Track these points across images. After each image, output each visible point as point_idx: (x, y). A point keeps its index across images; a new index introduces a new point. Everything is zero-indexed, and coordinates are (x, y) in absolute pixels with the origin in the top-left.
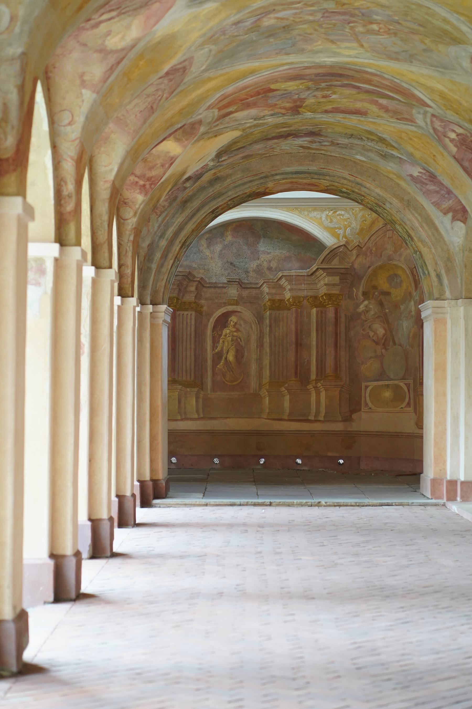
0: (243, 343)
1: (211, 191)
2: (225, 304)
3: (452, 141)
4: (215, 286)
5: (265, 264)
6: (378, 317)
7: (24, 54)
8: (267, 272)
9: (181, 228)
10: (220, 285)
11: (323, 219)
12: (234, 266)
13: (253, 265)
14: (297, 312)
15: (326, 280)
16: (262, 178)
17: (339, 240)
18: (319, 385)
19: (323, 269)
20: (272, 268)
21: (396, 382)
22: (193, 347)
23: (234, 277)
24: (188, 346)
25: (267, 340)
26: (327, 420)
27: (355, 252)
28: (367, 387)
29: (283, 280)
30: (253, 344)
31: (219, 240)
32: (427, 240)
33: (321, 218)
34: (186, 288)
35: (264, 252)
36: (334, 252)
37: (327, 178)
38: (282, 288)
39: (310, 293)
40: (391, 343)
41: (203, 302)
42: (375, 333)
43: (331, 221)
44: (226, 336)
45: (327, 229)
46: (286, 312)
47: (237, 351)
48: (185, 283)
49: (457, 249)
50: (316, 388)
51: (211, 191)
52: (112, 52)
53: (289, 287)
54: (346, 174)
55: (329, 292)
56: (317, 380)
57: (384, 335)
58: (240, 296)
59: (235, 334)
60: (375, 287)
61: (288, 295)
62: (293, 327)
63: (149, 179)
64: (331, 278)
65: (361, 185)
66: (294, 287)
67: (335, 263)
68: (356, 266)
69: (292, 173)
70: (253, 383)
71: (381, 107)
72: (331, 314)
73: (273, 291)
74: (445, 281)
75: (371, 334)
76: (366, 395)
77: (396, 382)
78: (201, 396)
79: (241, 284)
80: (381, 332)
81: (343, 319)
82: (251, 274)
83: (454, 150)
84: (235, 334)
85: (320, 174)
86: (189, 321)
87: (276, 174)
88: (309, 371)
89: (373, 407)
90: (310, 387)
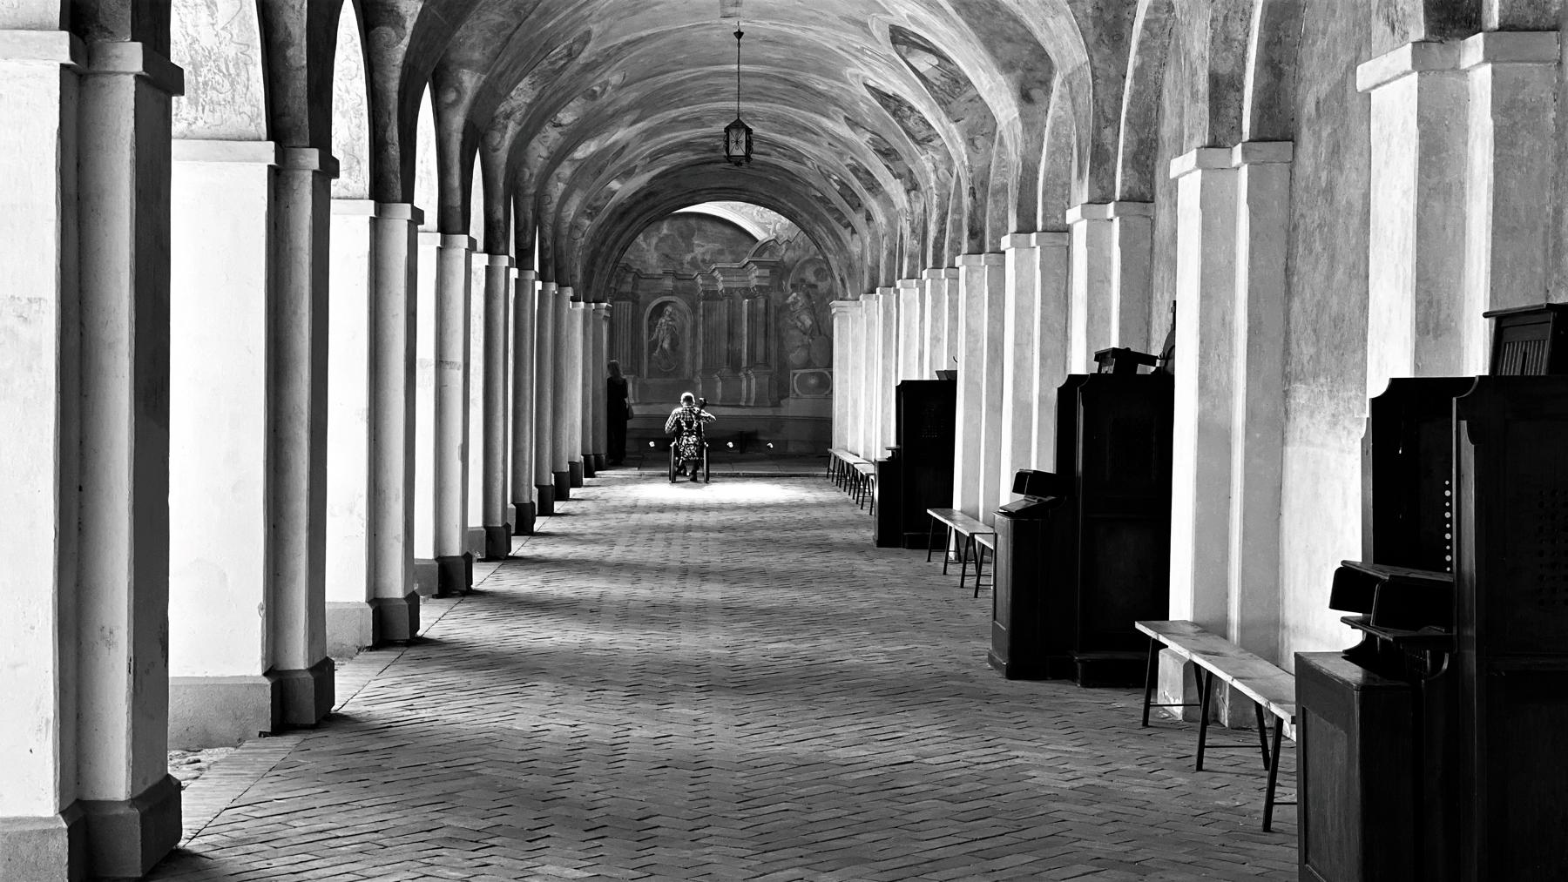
0: (677, 332)
1: (645, 205)
2: (661, 295)
3: (835, 181)
4: (511, 832)
5: (699, 257)
6: (806, 308)
7: (536, 192)
8: (701, 264)
9: (620, 236)
10: (656, 277)
11: (755, 214)
12: (670, 258)
13: (688, 257)
14: (729, 302)
15: (757, 273)
16: (690, 192)
17: (769, 234)
18: (750, 372)
19: (754, 262)
20: (705, 260)
21: (821, 370)
22: (630, 335)
23: (670, 269)
24: (625, 335)
25: (700, 329)
26: (759, 403)
27: (784, 246)
28: (794, 375)
29: (717, 272)
30: (688, 333)
31: (655, 233)
32: (832, 248)
33: (752, 214)
34: (623, 279)
35: (698, 245)
36: (765, 246)
37: (747, 193)
38: (715, 280)
39: (741, 285)
40: (817, 334)
41: (639, 292)
42: (803, 324)
43: (762, 217)
44: (661, 325)
45: (758, 224)
46: (718, 302)
47: (672, 339)
48: (623, 274)
49: (856, 257)
50: (746, 375)
51: (645, 205)
52: (577, 160)
53: (722, 279)
54: (762, 190)
55: (760, 284)
56: (748, 368)
57: (811, 326)
58: (675, 287)
59: (670, 323)
60: (803, 280)
61: (721, 287)
62: (726, 318)
63: (595, 208)
64: (761, 271)
65: (776, 200)
66: (727, 279)
67: (766, 257)
68: (785, 259)
69: (716, 189)
70: (687, 369)
71: (779, 153)
72: (761, 305)
73: (707, 282)
74: (848, 285)
75: (799, 324)
76: (794, 383)
77: (821, 370)
78: (638, 382)
79: (676, 276)
80: (808, 322)
81: (773, 311)
82: (686, 266)
83: (838, 187)
84: (670, 323)
85: (740, 190)
86: (626, 310)
87: (702, 190)
88: (740, 359)
89: (799, 393)
90: (741, 374)
